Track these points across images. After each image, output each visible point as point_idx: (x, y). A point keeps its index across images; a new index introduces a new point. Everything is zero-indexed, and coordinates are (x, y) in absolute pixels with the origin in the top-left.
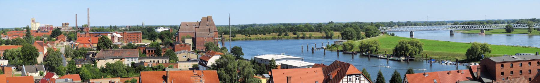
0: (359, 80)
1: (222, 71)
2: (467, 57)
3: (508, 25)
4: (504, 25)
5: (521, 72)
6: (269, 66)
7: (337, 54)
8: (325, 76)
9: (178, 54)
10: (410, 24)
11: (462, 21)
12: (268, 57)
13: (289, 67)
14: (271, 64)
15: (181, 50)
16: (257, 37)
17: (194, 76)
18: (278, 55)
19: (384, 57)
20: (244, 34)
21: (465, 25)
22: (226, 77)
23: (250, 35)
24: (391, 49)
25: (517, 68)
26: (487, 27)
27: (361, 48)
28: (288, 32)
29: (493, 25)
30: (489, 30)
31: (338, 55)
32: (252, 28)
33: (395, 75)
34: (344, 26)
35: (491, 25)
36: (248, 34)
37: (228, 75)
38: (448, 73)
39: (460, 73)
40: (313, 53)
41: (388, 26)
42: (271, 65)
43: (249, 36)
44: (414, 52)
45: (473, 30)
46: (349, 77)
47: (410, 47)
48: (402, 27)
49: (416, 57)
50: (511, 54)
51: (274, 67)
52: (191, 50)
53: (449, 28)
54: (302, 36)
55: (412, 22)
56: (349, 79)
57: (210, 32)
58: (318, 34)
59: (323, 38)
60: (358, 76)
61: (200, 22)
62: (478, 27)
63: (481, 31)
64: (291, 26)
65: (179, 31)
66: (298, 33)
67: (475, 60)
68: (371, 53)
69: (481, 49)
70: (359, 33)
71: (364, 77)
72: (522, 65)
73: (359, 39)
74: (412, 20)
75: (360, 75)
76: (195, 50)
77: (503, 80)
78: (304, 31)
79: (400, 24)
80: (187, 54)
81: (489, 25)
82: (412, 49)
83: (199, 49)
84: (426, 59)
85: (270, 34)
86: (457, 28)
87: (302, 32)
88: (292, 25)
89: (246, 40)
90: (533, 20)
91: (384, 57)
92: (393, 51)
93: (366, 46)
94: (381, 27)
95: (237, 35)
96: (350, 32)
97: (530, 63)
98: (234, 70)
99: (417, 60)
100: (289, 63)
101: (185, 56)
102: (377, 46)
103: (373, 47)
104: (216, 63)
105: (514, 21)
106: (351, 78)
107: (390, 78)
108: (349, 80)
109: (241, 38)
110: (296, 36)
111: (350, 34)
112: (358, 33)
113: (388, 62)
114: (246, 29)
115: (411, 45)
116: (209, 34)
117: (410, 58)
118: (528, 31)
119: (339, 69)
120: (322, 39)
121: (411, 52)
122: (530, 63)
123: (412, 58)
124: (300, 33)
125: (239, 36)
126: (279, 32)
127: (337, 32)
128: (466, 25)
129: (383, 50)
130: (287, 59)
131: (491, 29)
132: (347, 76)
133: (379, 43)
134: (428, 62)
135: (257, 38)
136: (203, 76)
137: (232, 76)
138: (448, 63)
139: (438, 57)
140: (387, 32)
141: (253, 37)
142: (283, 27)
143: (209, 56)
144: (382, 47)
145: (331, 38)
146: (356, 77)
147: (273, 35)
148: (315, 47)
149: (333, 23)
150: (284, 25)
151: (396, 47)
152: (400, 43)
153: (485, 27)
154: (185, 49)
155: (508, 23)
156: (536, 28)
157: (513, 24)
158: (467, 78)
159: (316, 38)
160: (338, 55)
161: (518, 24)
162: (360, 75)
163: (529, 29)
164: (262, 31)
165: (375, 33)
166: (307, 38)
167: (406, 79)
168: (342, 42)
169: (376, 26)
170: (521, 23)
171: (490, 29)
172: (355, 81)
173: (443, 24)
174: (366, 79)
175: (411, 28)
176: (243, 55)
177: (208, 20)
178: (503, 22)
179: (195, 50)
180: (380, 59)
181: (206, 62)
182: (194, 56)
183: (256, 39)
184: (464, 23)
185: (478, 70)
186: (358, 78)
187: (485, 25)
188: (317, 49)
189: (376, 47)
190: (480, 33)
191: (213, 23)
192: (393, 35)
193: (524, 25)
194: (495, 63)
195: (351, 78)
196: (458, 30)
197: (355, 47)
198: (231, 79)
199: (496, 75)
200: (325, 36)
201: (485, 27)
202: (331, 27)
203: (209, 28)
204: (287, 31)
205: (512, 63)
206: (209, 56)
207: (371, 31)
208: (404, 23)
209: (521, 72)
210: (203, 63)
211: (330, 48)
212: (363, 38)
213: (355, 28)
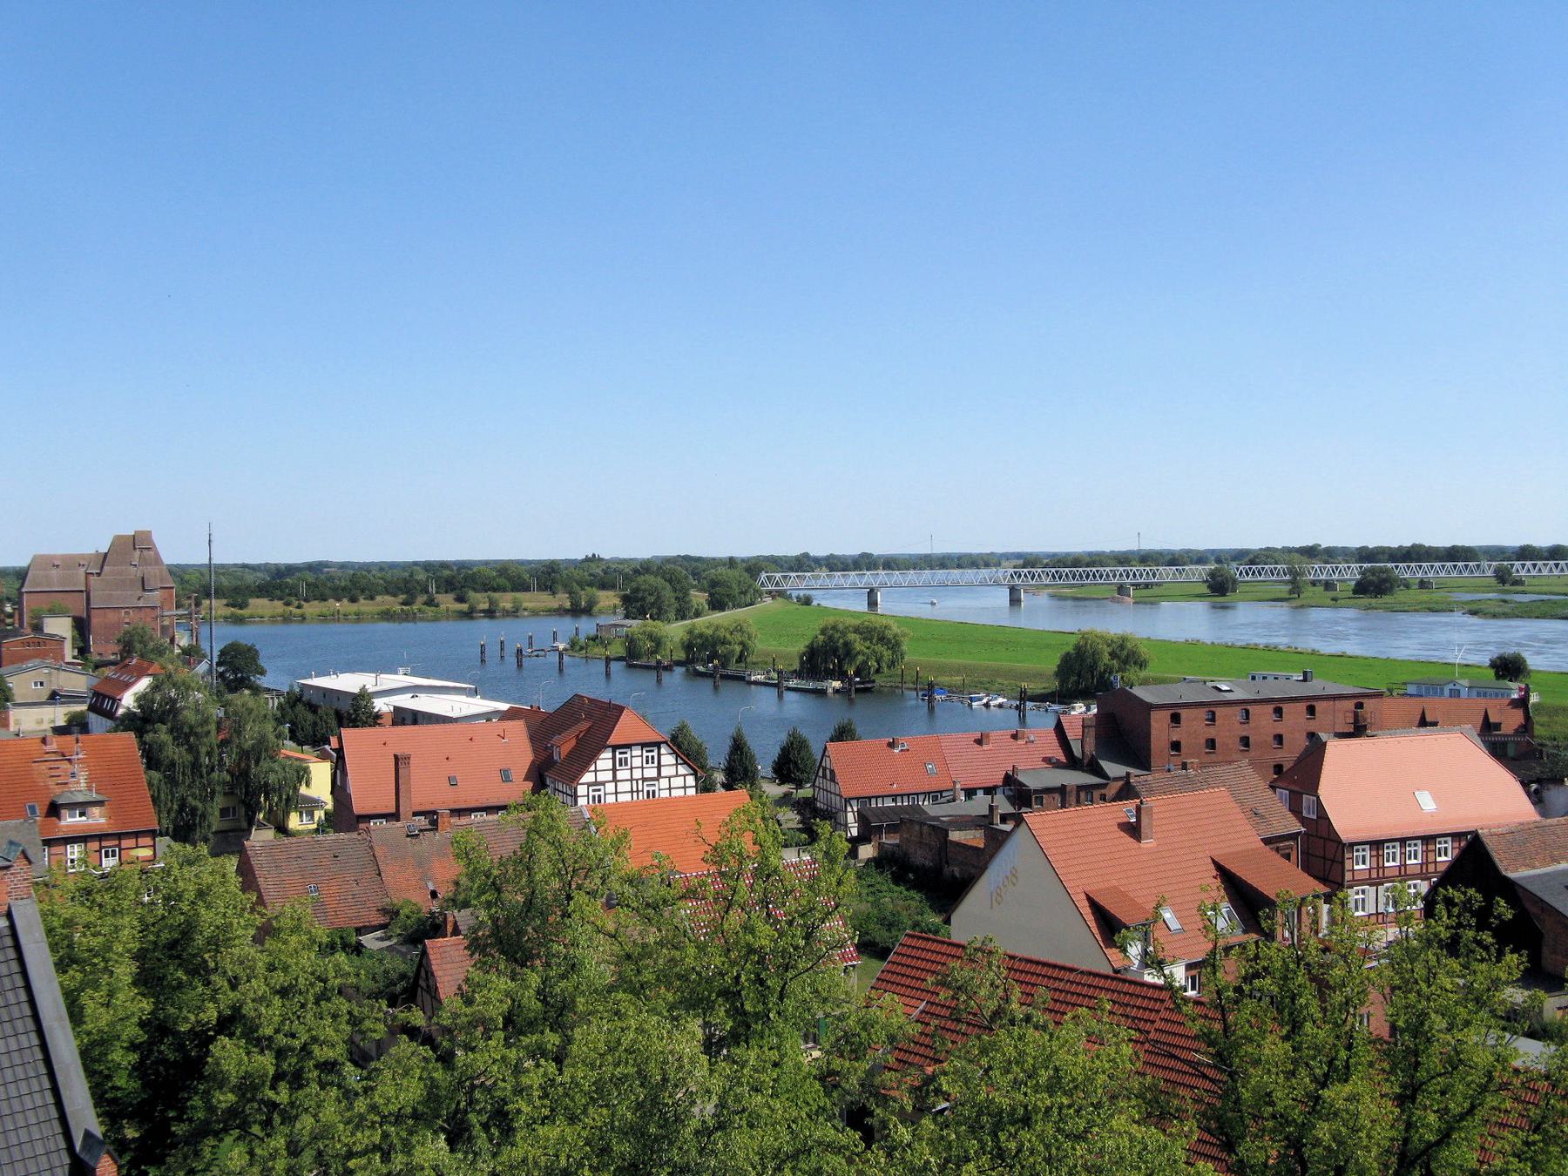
0: (656, 765)
1: (162, 734)
2: (1061, 685)
3: (1216, 569)
4: (1202, 571)
5: (1245, 741)
6: (348, 713)
7: (603, 669)
8: (535, 751)
9: (11, 674)
10: (869, 563)
11: (1055, 555)
12: (348, 682)
13: (420, 718)
14: (357, 708)
15: (24, 658)
16: (325, 611)
17: (47, 757)
18: (382, 676)
19: (769, 679)
20: (281, 599)
21: (1061, 570)
22: (176, 757)
23: (302, 603)
24: (795, 648)
25: (1228, 727)
26: (1141, 576)
27: (688, 647)
28: (437, 592)
29: (1161, 568)
30: (1147, 586)
31: (608, 675)
32: (311, 578)
33: (792, 743)
34: (636, 571)
35: (1155, 568)
36: (293, 599)
37: (183, 749)
38: (979, 742)
39: (1020, 742)
40: (520, 665)
41: (791, 569)
42: (355, 710)
43: (296, 603)
44: (873, 663)
45: (1090, 584)
46: (620, 753)
47: (859, 645)
48: (839, 573)
49: (879, 681)
50: (1209, 675)
51: (369, 720)
52: (69, 659)
53: (1004, 580)
54: (486, 606)
55: (879, 557)
56: (620, 760)
57: (144, 590)
58: (545, 600)
59: (560, 615)
60: (652, 751)
61: (106, 554)
62: (1108, 575)
63: (1119, 588)
64: (452, 570)
65: (23, 590)
66: (471, 594)
67: (1085, 695)
68: (724, 666)
69: (1110, 654)
70: (686, 594)
71: (675, 752)
72: (1247, 718)
73: (684, 618)
74: (879, 549)
75: (658, 745)
76: (86, 659)
77: (1169, 771)
78: (495, 590)
79: (834, 564)
80: (50, 673)
81: (1148, 569)
82: (866, 651)
83: (100, 654)
84: (916, 689)
85: (372, 598)
86: (1032, 579)
87: (486, 591)
88: (455, 568)
89: (287, 619)
90: (1311, 552)
91: (769, 679)
92: (801, 658)
93: (707, 638)
94: (763, 575)
95: (252, 601)
96: (654, 591)
97: (1278, 711)
98: (206, 729)
99: (886, 689)
100: (425, 704)
101: (42, 684)
102: (745, 639)
103: (730, 644)
104: (139, 707)
105: (1239, 555)
106: (626, 759)
107: (774, 753)
108: (653, 757)
109: (268, 612)
110: (464, 607)
111: (652, 599)
112: (681, 595)
113: (780, 696)
114: (288, 580)
115: (865, 639)
116: (139, 598)
117: (858, 683)
118: (1291, 592)
119: (584, 726)
120: (557, 618)
121: (865, 662)
122: (1278, 711)
123: (869, 682)
124: (479, 595)
125: (259, 605)
126: (407, 593)
127: (611, 593)
128: (1067, 570)
129: (768, 655)
130: (415, 690)
131: (1157, 584)
132: (614, 752)
133: (753, 630)
134: (923, 700)
135: (328, 613)
136: (80, 756)
137: (198, 753)
138: (992, 703)
139: (958, 679)
140: (785, 591)
141: (312, 608)
142: (421, 576)
143: (125, 678)
144: (762, 645)
145: (590, 615)
146: (645, 754)
147: (386, 602)
148: (531, 644)
149: (600, 560)
150: (428, 566)
151: (812, 643)
152: (823, 632)
153: (1134, 575)
154: (43, 655)
155: (1218, 561)
156: (1320, 581)
157: (1235, 566)
158: (1047, 760)
159: (535, 613)
160: (608, 675)
161: (1254, 567)
162: (658, 745)
163: (1293, 582)
164: (344, 589)
165: (744, 593)
166: (508, 614)
167: (828, 759)
168: (622, 626)
169: (748, 570)
170: (1266, 564)
171: (1152, 584)
172: (642, 768)
173: (987, 565)
174: (680, 761)
175: (869, 578)
176: (263, 673)
177: (138, 544)
178: (1200, 558)
179: (86, 659)
180: (753, 686)
181: (116, 701)
182: (79, 682)
183: (323, 618)
184: (1059, 561)
185: (1086, 730)
186: (653, 757)
187: (1134, 569)
188: (535, 653)
189: (741, 643)
190: (1113, 598)
191: (157, 554)
192: (807, 601)
193: (1275, 569)
194: (1151, 707)
195: (628, 755)
196: (1037, 587)
197: (669, 646)
198: (196, 766)
199: (1152, 752)
200: (568, 605)
201: (1134, 575)
202: (591, 575)
203: (139, 574)
204: (432, 589)
205: (1211, 710)
206: (125, 678)
207: (728, 587)
208: (850, 561)
209: (1245, 741)
210: (102, 702)
211: (582, 648)
212: (698, 614)
213: (671, 579)
